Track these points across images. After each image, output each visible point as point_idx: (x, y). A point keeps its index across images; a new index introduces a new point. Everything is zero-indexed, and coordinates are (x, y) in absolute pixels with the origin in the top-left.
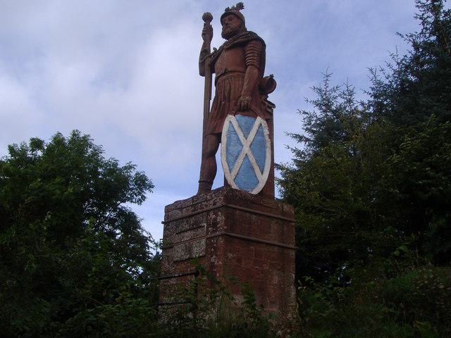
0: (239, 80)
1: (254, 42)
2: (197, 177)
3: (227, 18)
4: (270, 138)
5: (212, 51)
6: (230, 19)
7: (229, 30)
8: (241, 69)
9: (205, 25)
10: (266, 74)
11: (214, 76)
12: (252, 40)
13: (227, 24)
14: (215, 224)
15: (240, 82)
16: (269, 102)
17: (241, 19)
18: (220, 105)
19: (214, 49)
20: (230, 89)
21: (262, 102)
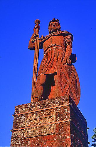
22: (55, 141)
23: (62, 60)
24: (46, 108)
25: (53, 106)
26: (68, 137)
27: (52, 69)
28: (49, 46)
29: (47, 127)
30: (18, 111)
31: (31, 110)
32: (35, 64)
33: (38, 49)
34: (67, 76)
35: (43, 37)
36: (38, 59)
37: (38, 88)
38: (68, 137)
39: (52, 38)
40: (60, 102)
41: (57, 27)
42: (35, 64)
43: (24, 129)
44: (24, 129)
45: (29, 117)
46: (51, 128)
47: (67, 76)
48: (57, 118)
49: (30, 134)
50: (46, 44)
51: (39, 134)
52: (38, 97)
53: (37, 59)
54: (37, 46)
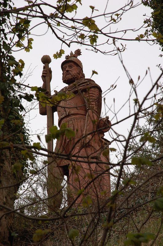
0: (81, 122)
1: (93, 89)
2: (20, 7)
3: (67, 65)
4: (50, 72)
5: (53, 93)
6: (70, 67)
7: (69, 77)
8: (82, 112)
9: (44, 68)
10: (103, 116)
11: (56, 114)
12: (91, 88)
13: (67, 71)
15: (82, 123)
16: (106, 140)
17: (79, 65)
18: (65, 143)
19: (55, 91)
21: (100, 140)
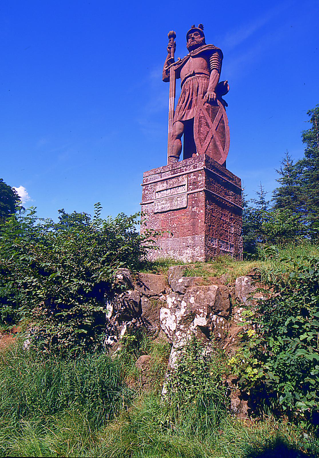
14: (195, 184)
20: (198, 86)
22: (187, 216)
23: (204, 96)
24: (177, 173)
25: (186, 170)
26: (202, 211)
27: (191, 110)
28: (186, 76)
29: (179, 199)
30: (147, 179)
31: (161, 176)
32: (171, 106)
33: (174, 79)
34: (209, 121)
35: (180, 61)
36: (175, 97)
37: (174, 142)
38: (202, 211)
39: (191, 61)
40: (194, 164)
41: (198, 39)
42: (171, 106)
43: (153, 202)
44: (153, 202)
45: (158, 187)
46: (183, 200)
47: (209, 121)
48: (190, 187)
49: (160, 208)
50: (184, 72)
51: (169, 208)
52: (173, 155)
53: (173, 97)
54: (172, 76)
